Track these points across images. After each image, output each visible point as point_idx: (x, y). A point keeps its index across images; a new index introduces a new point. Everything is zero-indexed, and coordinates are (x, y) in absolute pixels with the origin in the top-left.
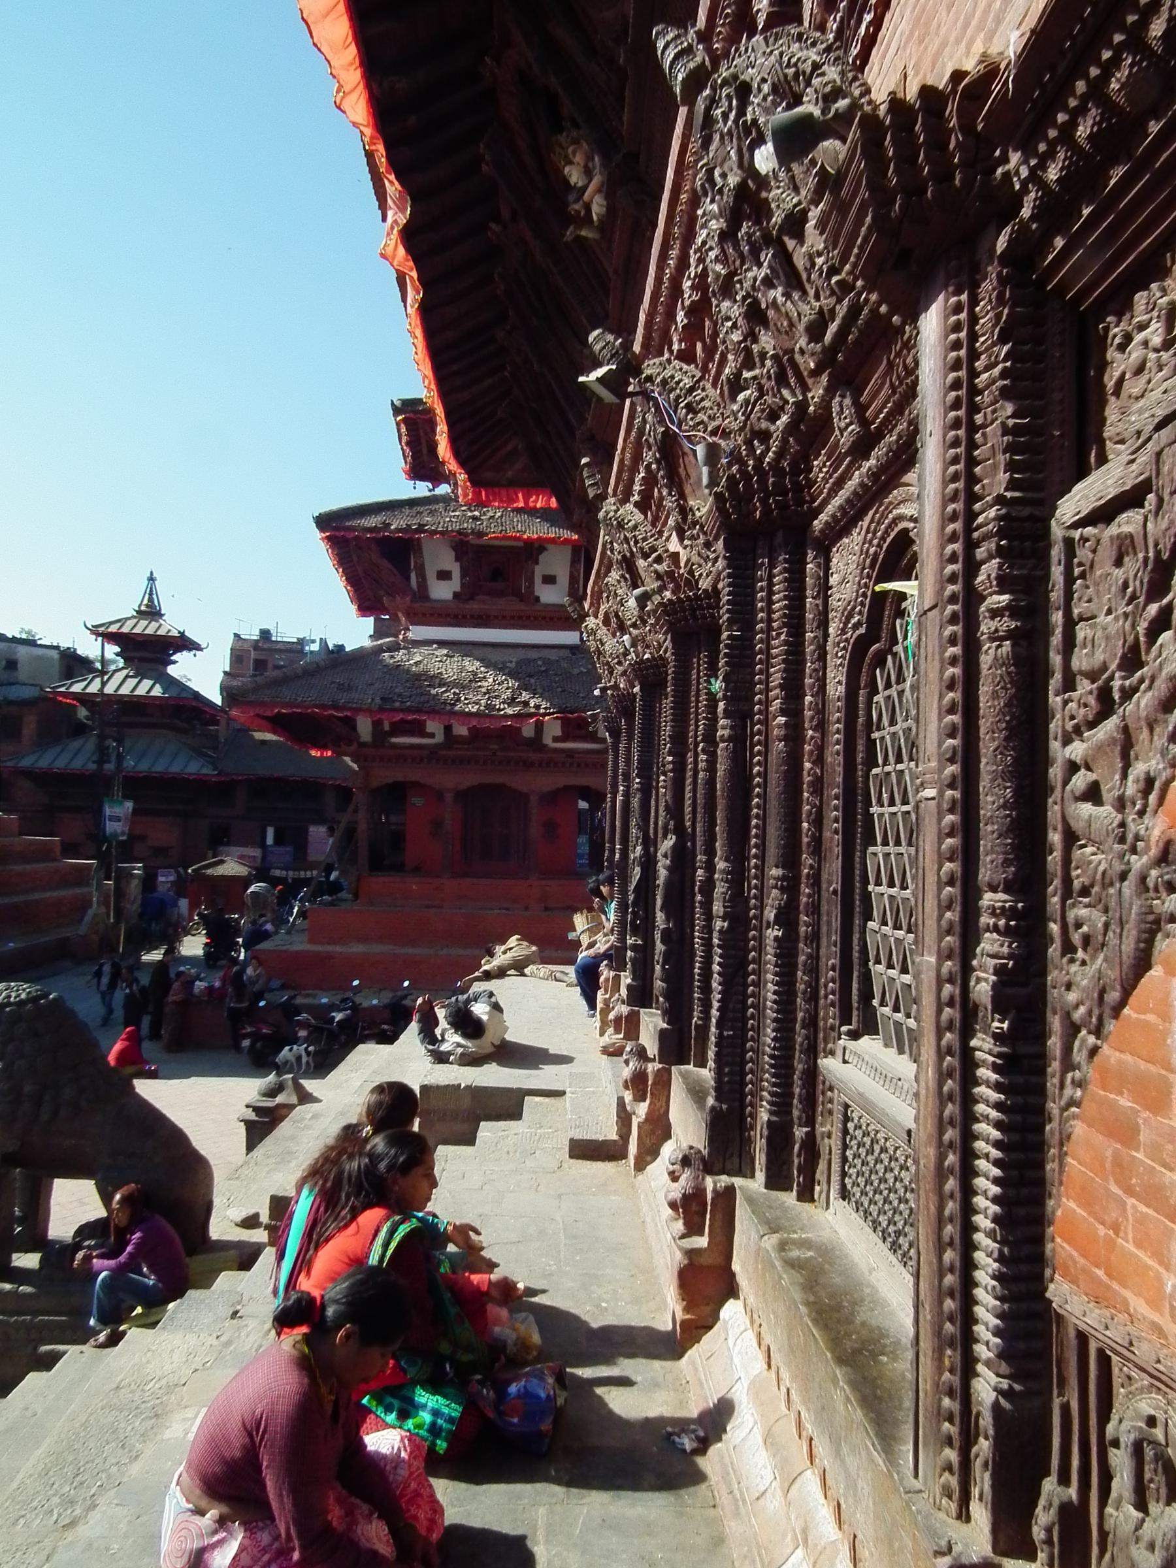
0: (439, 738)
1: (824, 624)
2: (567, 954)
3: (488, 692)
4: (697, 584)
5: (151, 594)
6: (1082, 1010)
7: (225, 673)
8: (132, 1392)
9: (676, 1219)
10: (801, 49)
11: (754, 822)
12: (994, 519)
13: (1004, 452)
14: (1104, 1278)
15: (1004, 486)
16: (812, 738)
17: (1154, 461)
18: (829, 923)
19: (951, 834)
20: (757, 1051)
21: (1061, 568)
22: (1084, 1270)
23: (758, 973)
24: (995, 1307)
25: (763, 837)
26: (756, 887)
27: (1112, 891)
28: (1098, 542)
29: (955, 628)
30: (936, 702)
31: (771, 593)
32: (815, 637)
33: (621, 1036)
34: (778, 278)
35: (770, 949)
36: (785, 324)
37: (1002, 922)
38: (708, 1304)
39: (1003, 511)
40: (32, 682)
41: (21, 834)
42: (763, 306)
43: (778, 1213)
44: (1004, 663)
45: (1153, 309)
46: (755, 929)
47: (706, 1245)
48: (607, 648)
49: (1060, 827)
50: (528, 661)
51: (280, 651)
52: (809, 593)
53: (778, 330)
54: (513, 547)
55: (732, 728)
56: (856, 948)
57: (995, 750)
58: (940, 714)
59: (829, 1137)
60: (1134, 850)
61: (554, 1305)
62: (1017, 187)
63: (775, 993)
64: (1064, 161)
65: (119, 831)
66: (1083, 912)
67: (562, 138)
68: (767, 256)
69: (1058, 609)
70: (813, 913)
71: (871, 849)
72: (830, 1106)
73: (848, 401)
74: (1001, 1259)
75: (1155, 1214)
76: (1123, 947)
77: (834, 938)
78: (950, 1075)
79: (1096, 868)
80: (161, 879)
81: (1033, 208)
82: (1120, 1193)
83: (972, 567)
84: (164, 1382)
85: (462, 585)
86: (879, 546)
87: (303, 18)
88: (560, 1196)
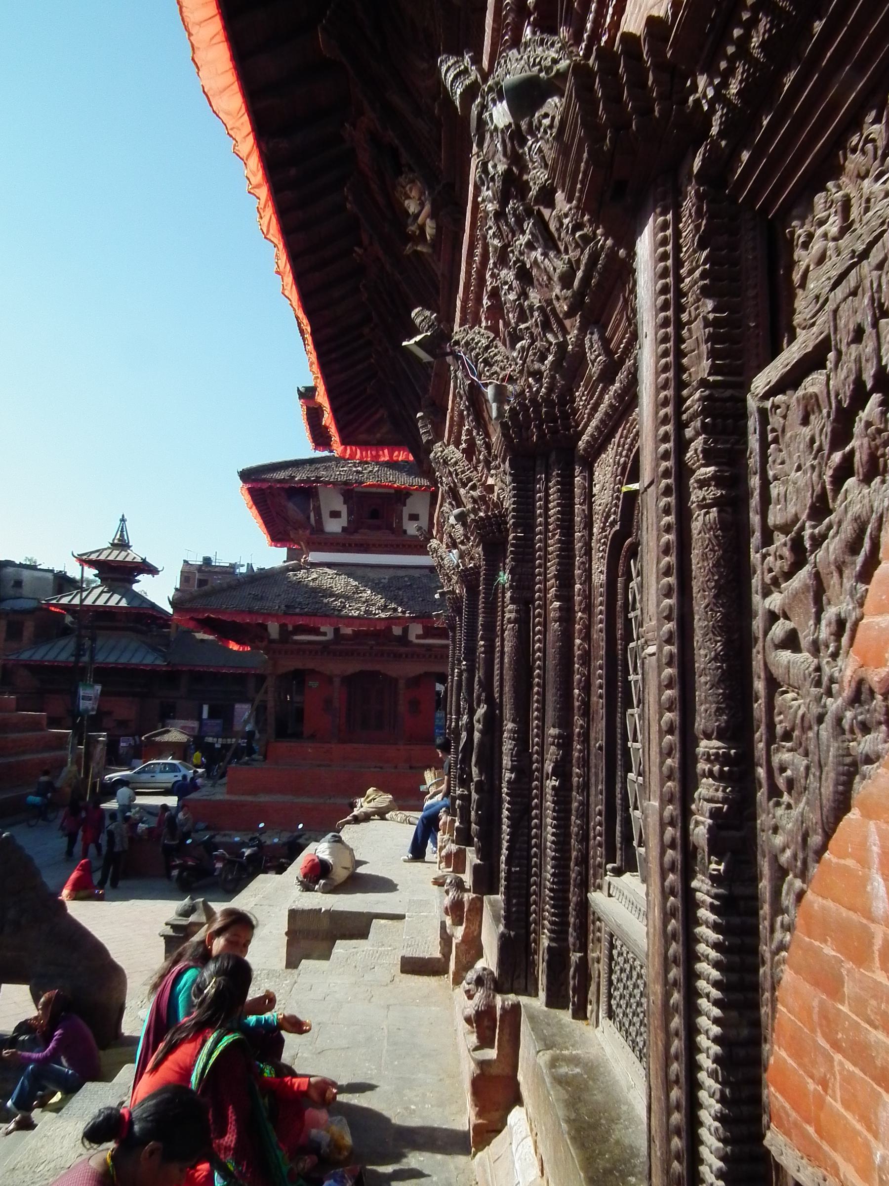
0: (330, 636)
1: (589, 524)
2: (412, 802)
3: (367, 601)
4: (502, 505)
5: (122, 531)
6: (788, 853)
7: (176, 589)
8: (25, 1173)
9: (473, 1032)
10: (544, 51)
11: (536, 689)
12: (699, 400)
13: (706, 342)
14: (815, 1136)
15: (707, 371)
16: (581, 618)
17: (831, 318)
18: (597, 775)
19: (669, 686)
20: (539, 885)
21: (757, 436)
22: (796, 1124)
23: (540, 817)
24: (718, 1149)
25: (543, 702)
26: (537, 744)
27: (811, 734)
28: (788, 407)
29: (669, 499)
30: (655, 566)
31: (547, 502)
32: (583, 536)
33: (451, 869)
34: (538, 241)
35: (549, 797)
36: (545, 278)
37: (716, 768)
38: (497, 1110)
39: (707, 393)
40: (31, 596)
41: (18, 710)
42: (528, 266)
43: (555, 1030)
44: (711, 528)
45: (830, 207)
46: (537, 779)
47: (495, 1057)
48: (446, 562)
49: (762, 675)
50: (398, 578)
51: (216, 573)
52: (577, 500)
53: (540, 285)
54: (386, 493)
55: (517, 611)
56: (619, 796)
57: (706, 607)
58: (657, 577)
59: (598, 962)
60: (829, 693)
61: (370, 1107)
62: (706, 108)
63: (553, 834)
64: (743, 74)
65: (90, 708)
66: (786, 756)
67: (402, 179)
68: (528, 225)
69: (755, 473)
70: (583, 766)
71: (630, 711)
72: (598, 934)
73: (596, 337)
74: (722, 1100)
75: (862, 1075)
76: (823, 790)
77: (600, 787)
78: (673, 915)
79: (796, 712)
80: (122, 744)
81: (720, 124)
82: (827, 1046)
83: (682, 445)
84: (52, 1165)
85: (349, 522)
86: (627, 456)
87: (204, 91)
88: (388, 1006)
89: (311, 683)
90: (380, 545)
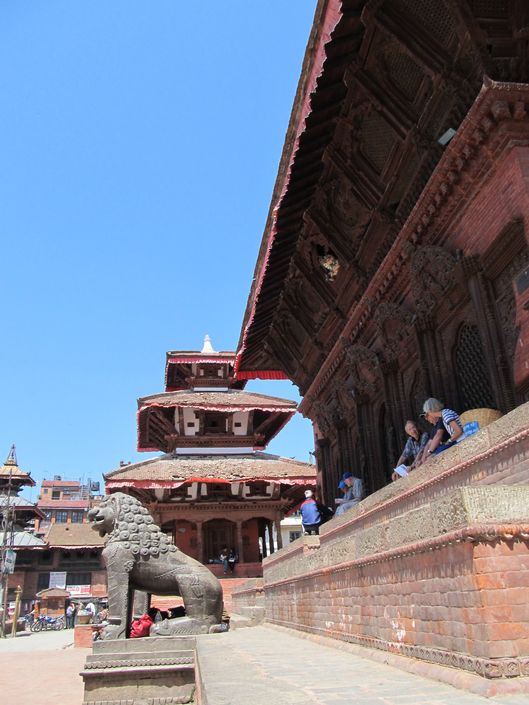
85: (200, 428)
89: (181, 530)
90: (219, 442)
